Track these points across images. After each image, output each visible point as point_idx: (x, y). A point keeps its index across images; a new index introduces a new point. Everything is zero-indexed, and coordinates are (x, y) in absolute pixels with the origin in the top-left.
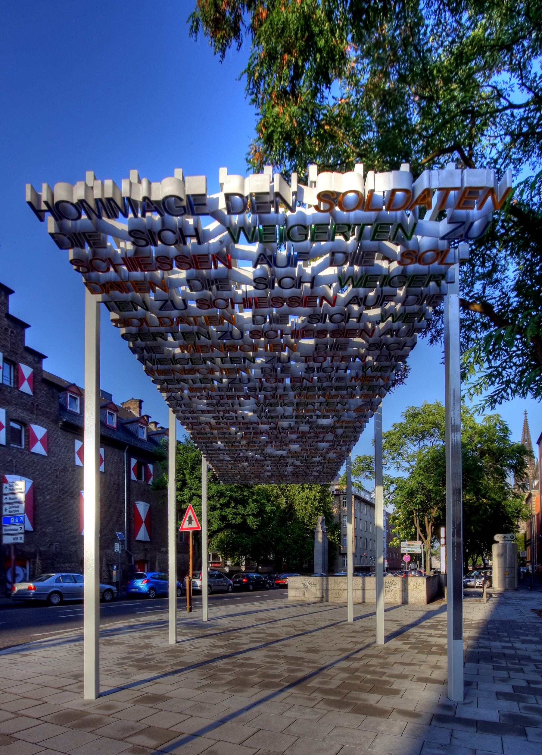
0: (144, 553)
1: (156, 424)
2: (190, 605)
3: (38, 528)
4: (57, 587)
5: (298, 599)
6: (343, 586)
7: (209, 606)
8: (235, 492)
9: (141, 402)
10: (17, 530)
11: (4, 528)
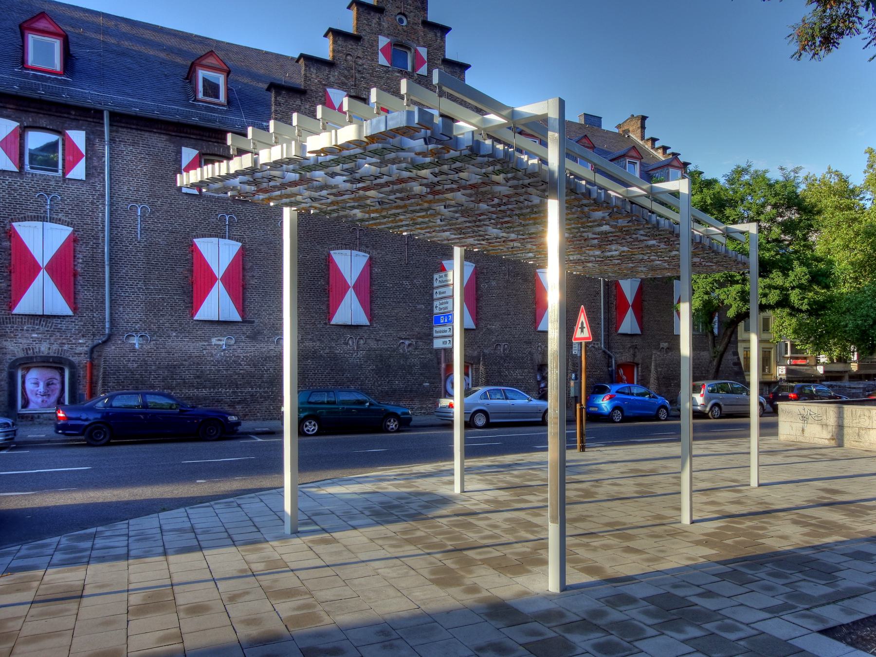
0: (632, 351)
1: (665, 148)
2: (582, 441)
3: (482, 324)
4: (483, 404)
5: (793, 438)
6: (865, 422)
7: (761, 435)
8: (769, 250)
9: (644, 118)
10: (445, 331)
11: (435, 329)
